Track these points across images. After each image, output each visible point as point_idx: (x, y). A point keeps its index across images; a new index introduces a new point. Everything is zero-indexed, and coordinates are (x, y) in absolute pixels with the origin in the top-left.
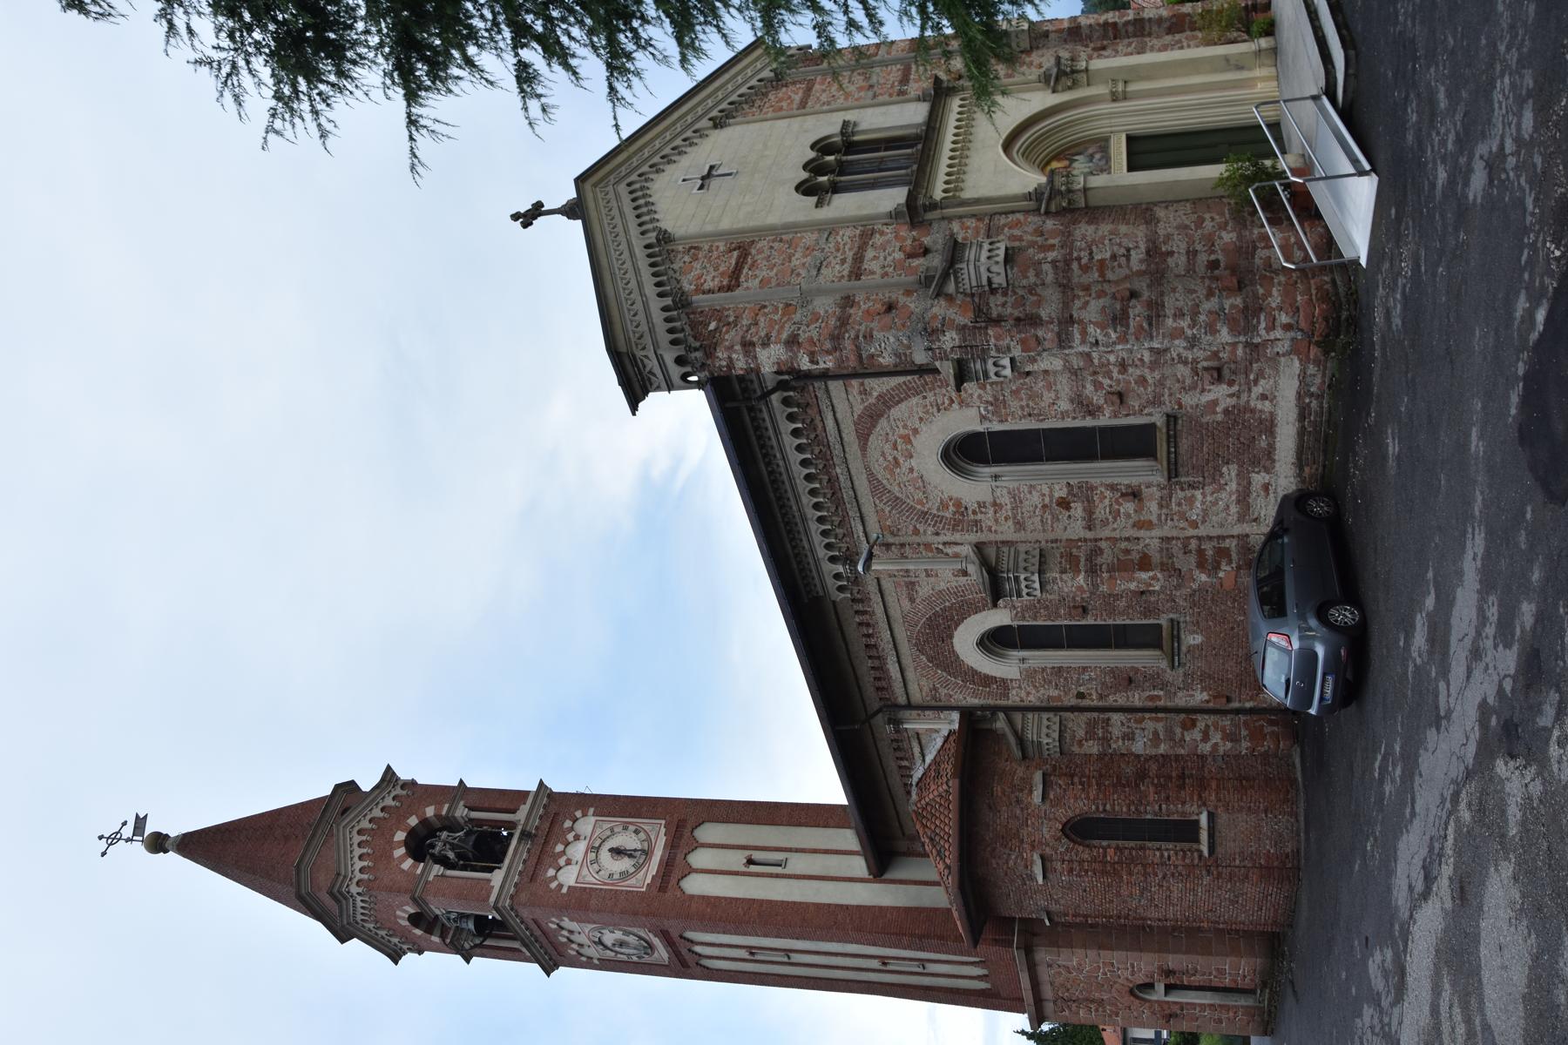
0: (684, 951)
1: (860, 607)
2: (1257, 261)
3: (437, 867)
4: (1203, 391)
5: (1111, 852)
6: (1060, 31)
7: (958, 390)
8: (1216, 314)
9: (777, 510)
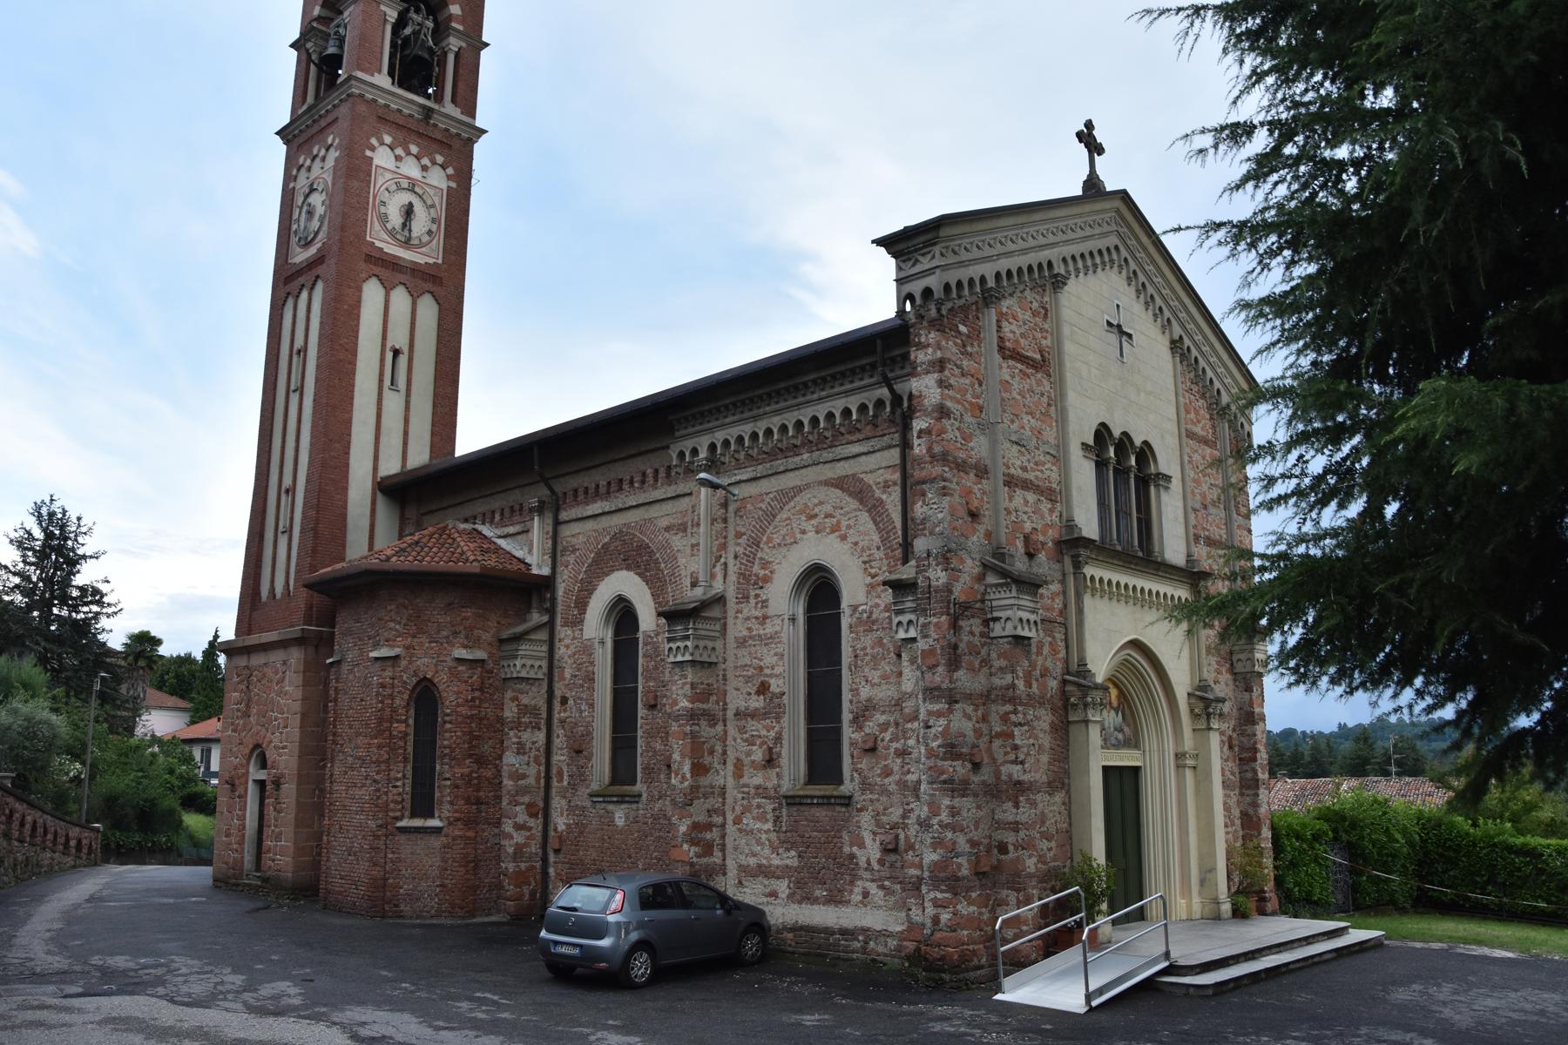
0: (301, 280)
1: (662, 474)
2: (1005, 892)
3: (395, 15)
4: (875, 834)
5: (402, 727)
6: (1251, 704)
7: (885, 583)
8: (952, 849)
9: (767, 390)
